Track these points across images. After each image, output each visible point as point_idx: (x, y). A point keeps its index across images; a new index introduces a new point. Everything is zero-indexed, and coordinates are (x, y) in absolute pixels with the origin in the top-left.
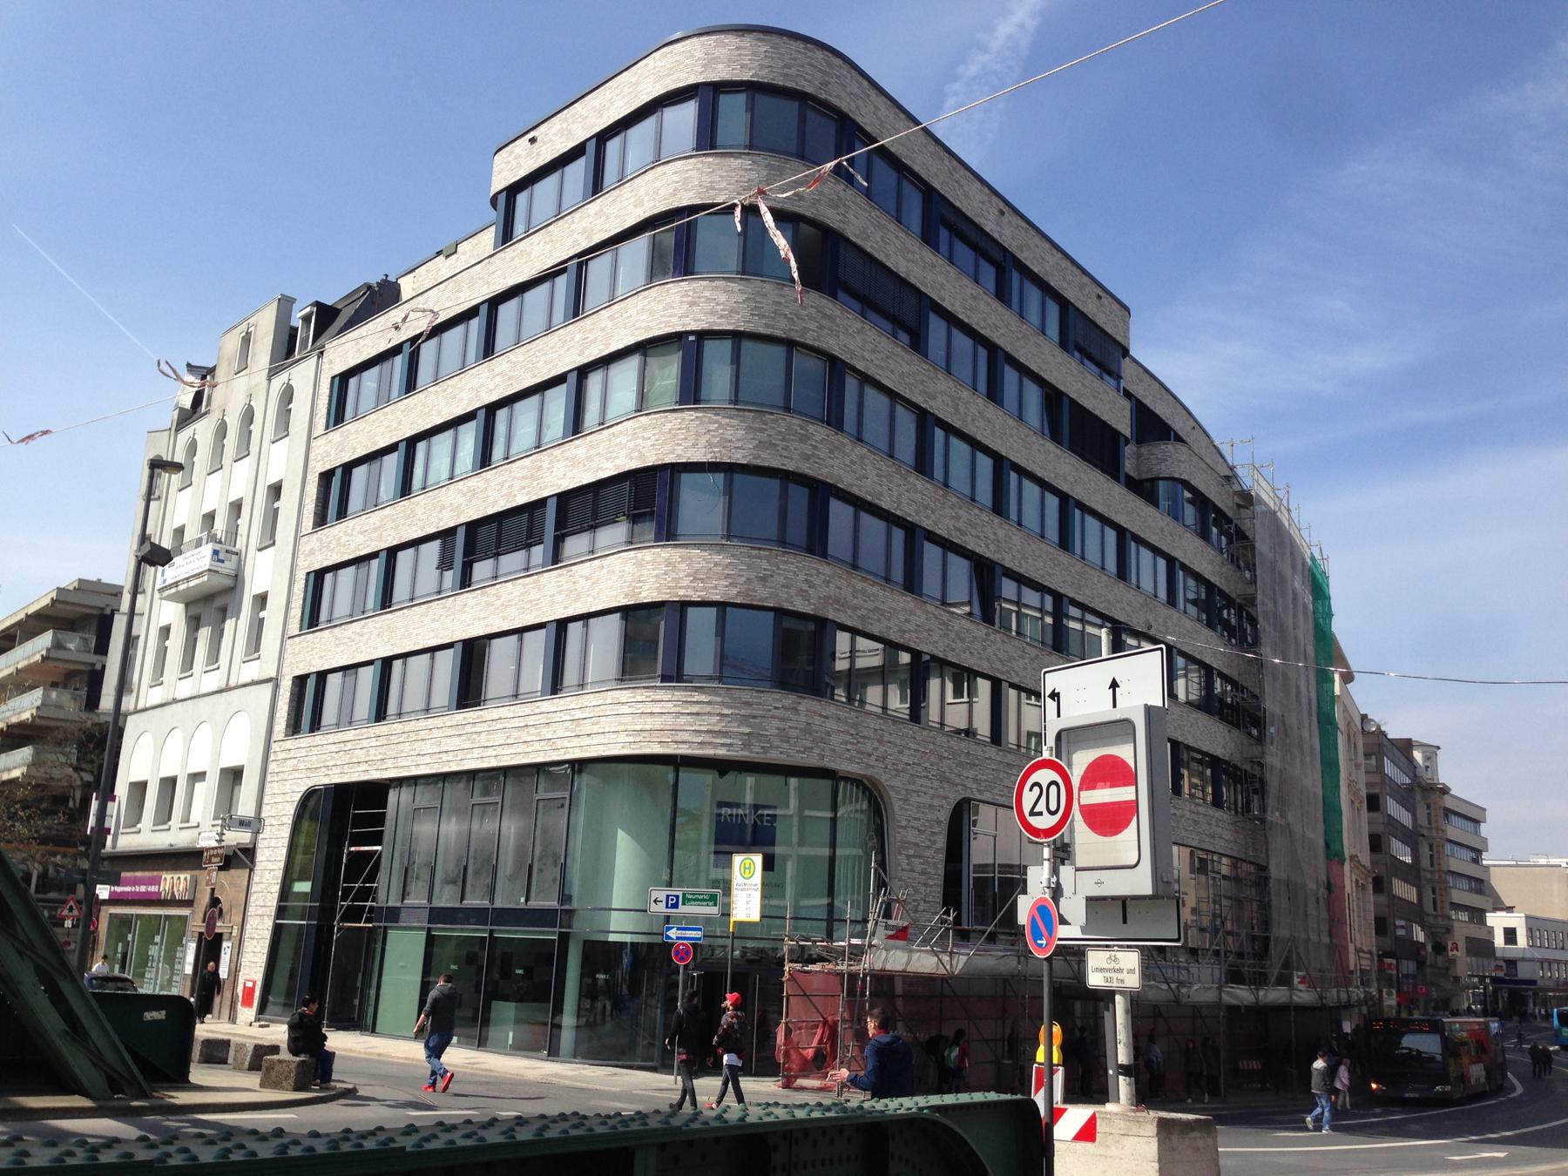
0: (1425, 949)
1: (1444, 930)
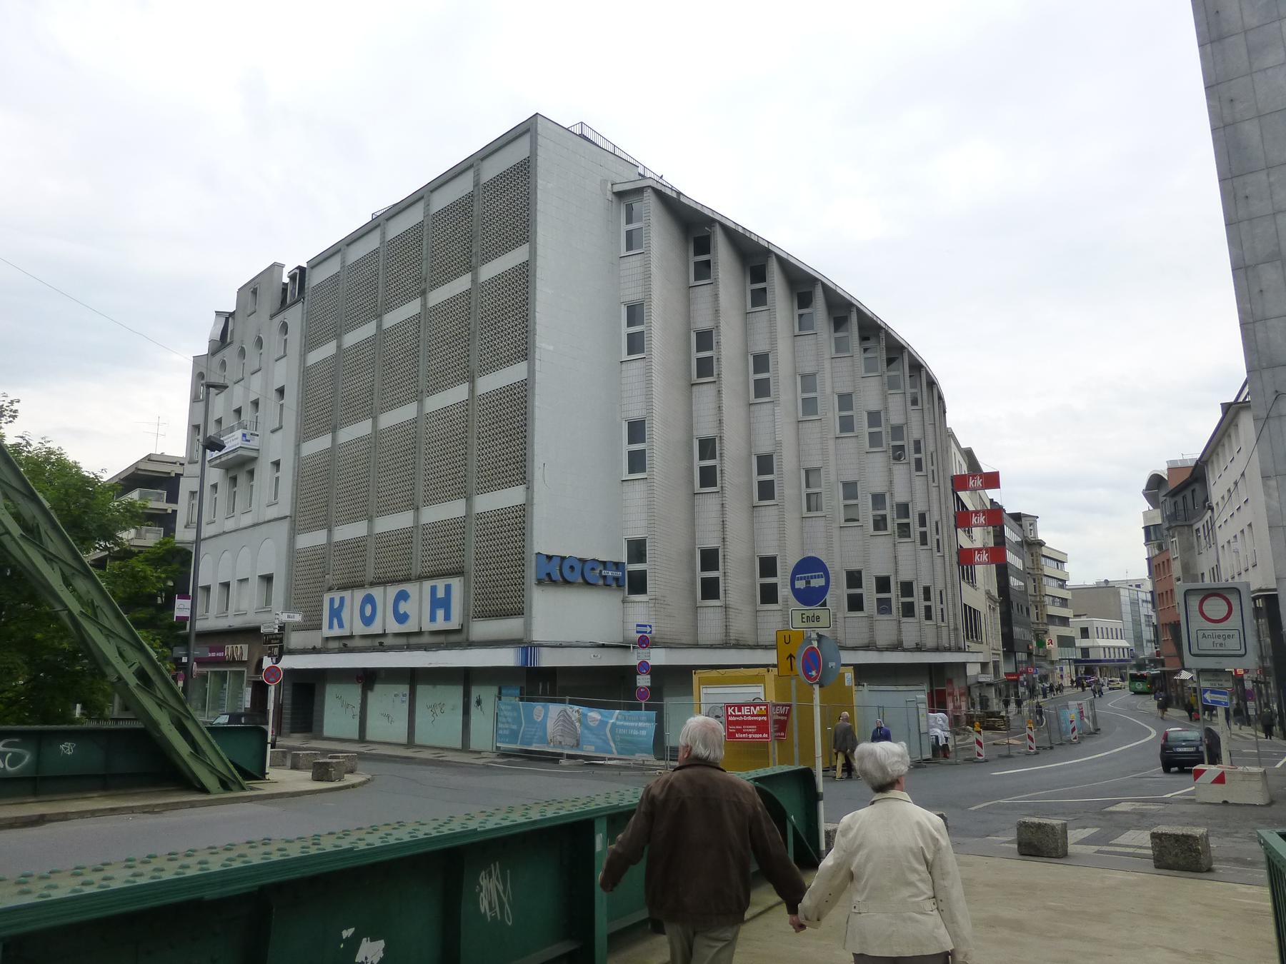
0: (1032, 645)
1: (1043, 632)
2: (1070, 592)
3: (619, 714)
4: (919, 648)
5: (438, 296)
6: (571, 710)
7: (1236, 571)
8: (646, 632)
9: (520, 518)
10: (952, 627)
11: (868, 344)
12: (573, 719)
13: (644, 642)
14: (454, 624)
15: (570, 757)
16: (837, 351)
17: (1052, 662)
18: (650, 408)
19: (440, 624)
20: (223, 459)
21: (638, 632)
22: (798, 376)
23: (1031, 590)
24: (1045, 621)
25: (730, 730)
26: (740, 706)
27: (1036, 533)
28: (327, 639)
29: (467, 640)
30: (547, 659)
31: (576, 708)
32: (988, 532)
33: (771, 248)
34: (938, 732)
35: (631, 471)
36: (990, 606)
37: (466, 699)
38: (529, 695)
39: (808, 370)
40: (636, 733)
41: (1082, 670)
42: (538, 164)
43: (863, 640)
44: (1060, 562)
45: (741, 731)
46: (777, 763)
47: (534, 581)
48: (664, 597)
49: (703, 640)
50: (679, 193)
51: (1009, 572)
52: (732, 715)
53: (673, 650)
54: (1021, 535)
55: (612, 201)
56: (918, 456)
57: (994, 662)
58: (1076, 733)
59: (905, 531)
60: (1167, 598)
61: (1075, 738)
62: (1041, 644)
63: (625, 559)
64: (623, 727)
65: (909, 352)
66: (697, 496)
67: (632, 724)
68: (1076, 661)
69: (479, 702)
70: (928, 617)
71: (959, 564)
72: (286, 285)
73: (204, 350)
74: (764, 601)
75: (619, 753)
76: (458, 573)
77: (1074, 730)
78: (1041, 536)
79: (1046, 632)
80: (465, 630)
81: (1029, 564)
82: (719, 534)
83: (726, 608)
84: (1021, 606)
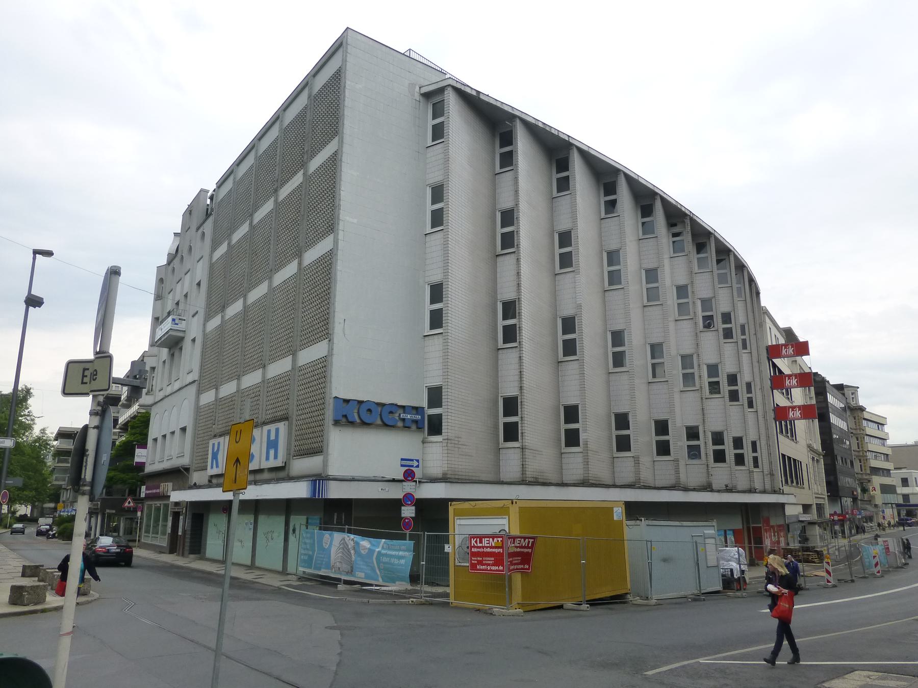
0: (857, 491)
1: (867, 481)
2: (890, 449)
3: (385, 543)
4: (729, 490)
5: (284, 192)
6: (348, 539)
8: (412, 466)
9: (322, 369)
10: (766, 472)
11: (676, 230)
12: (350, 547)
13: (409, 476)
14: (279, 463)
15: (347, 582)
16: (644, 234)
17: (876, 506)
18: (446, 272)
19: (272, 463)
20: (162, 339)
21: (402, 466)
22: (604, 252)
23: (855, 447)
25: (473, 562)
26: (481, 537)
28: (212, 476)
29: (288, 475)
30: (335, 491)
31: (352, 536)
32: (810, 398)
33: (571, 141)
34: (734, 565)
35: (432, 327)
36: (813, 458)
37: (286, 527)
38: (327, 525)
39: (613, 247)
40: (396, 562)
41: (903, 513)
42: (347, 68)
43: (671, 481)
44: (880, 425)
45: (480, 563)
47: (331, 422)
48: (458, 438)
49: (504, 477)
50: (478, 92)
51: (833, 430)
52: (474, 547)
53: (455, 484)
54: (844, 402)
55: (419, 101)
56: (743, 337)
58: (879, 568)
59: (716, 389)
61: (879, 572)
62: (864, 490)
63: (425, 404)
64: (386, 555)
65: (715, 237)
66: (500, 352)
67: (394, 553)
68: (898, 505)
69: (294, 531)
70: (756, 465)
71: (775, 419)
72: (208, 205)
73: (164, 262)
74: (568, 444)
75: (383, 580)
76: (285, 418)
77: (876, 565)
79: (869, 481)
80: (287, 468)
81: (852, 425)
82: (517, 384)
83: (522, 449)
84: (845, 459)
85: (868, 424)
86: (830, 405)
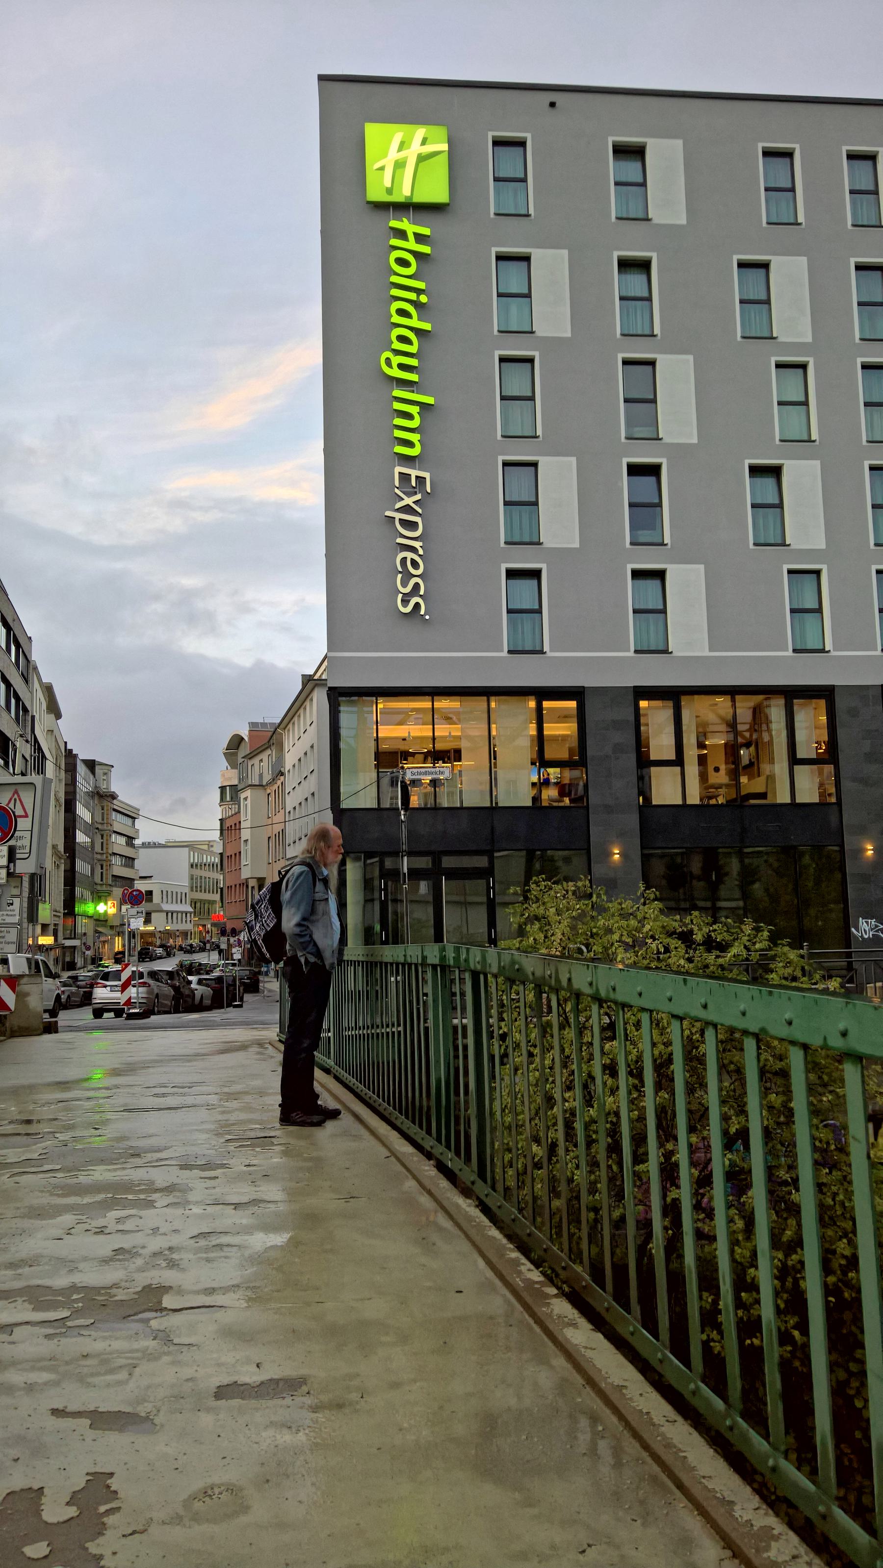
7: (304, 833)
23: (98, 848)
24: (110, 882)
27: (108, 784)
46: (198, 872)
51: (78, 825)
57: (55, 925)
60: (235, 894)
78: (114, 788)
85: (116, 839)
86: (78, 819)
